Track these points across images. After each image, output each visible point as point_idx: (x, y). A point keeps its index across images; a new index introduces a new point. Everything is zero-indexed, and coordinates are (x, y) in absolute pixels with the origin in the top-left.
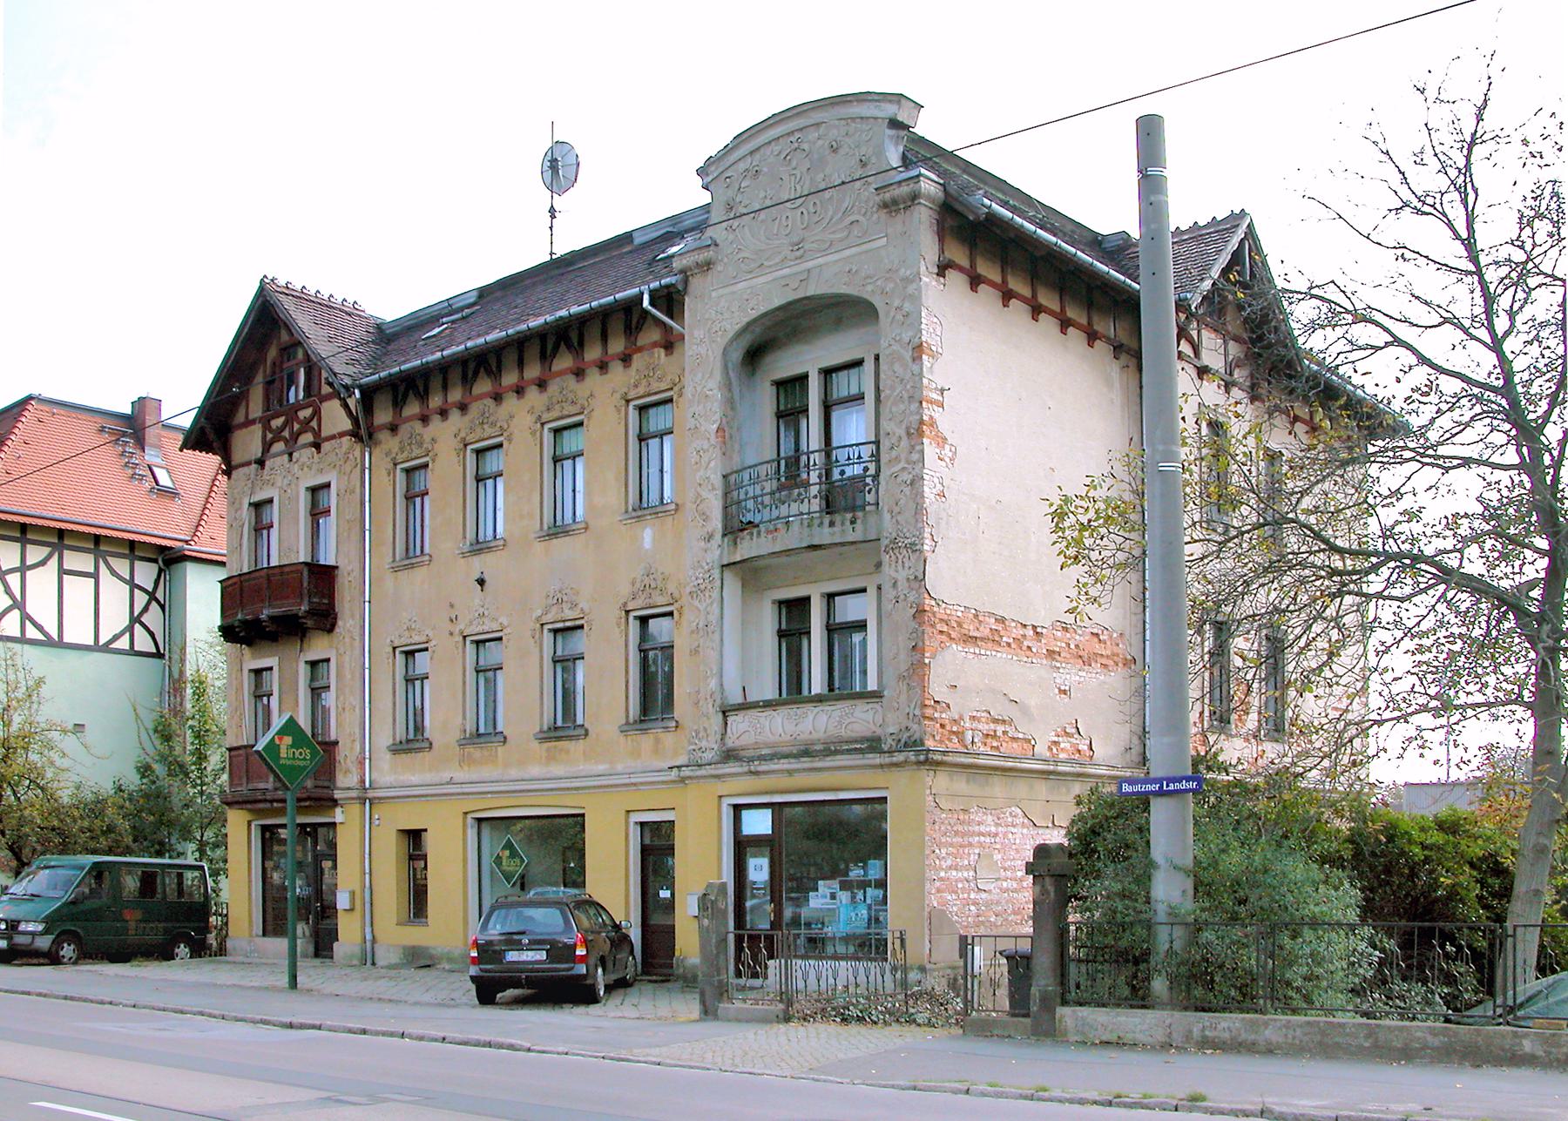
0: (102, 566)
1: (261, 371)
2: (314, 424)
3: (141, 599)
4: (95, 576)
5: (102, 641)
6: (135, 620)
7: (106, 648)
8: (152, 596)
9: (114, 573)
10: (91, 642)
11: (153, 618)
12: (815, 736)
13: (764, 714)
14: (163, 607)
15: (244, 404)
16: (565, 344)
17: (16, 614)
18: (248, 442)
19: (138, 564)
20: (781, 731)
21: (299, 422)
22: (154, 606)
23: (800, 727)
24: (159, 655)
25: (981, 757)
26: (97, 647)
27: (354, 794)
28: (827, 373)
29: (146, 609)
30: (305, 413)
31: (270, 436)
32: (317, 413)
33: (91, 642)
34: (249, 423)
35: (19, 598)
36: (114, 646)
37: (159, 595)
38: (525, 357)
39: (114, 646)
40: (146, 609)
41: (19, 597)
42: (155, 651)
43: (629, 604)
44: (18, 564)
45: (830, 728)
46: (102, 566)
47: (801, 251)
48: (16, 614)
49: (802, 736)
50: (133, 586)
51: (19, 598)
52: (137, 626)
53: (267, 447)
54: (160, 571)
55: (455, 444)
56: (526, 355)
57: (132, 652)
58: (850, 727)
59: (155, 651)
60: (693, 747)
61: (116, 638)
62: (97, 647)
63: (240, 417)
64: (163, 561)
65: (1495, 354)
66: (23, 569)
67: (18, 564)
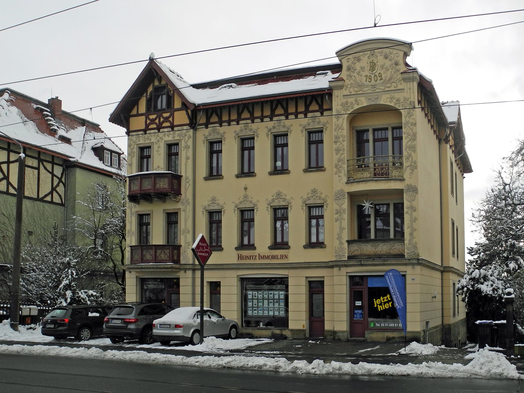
0: (41, 165)
1: (145, 95)
2: (171, 119)
3: (56, 181)
4: (38, 169)
5: (41, 196)
6: (53, 189)
7: (42, 200)
8: (60, 180)
9: (46, 168)
10: (36, 197)
11: (61, 189)
12: (382, 253)
13: (364, 244)
14: (64, 185)
15: (136, 107)
16: (315, 100)
17: (4, 182)
18: (138, 123)
19: (55, 166)
20: (370, 250)
21: (163, 117)
22: (61, 184)
23: (377, 249)
24: (62, 205)
25: (411, 260)
26: (38, 199)
27: (191, 267)
28: (374, 130)
29: (58, 185)
30: (165, 115)
31: (148, 122)
32: (172, 115)
33: (36, 197)
34: (138, 115)
35: (6, 175)
36: (45, 199)
37: (63, 180)
38: (231, 113)
39: (45, 199)
40: (58, 185)
41: (6, 174)
42: (61, 203)
43: (307, 201)
44: (6, 160)
45: (387, 250)
46: (41, 165)
47: (375, 89)
48: (4, 182)
49: (378, 253)
50: (53, 175)
51: (6, 175)
52: (54, 192)
53: (147, 126)
54: (64, 170)
55: (266, 131)
56: (264, 108)
57: (52, 202)
58: (393, 250)
59: (61, 203)
60: (337, 254)
61: (46, 196)
62: (38, 199)
63: (134, 112)
64: (65, 166)
65: (10, 181)
66: (8, 162)
67: (6, 160)
